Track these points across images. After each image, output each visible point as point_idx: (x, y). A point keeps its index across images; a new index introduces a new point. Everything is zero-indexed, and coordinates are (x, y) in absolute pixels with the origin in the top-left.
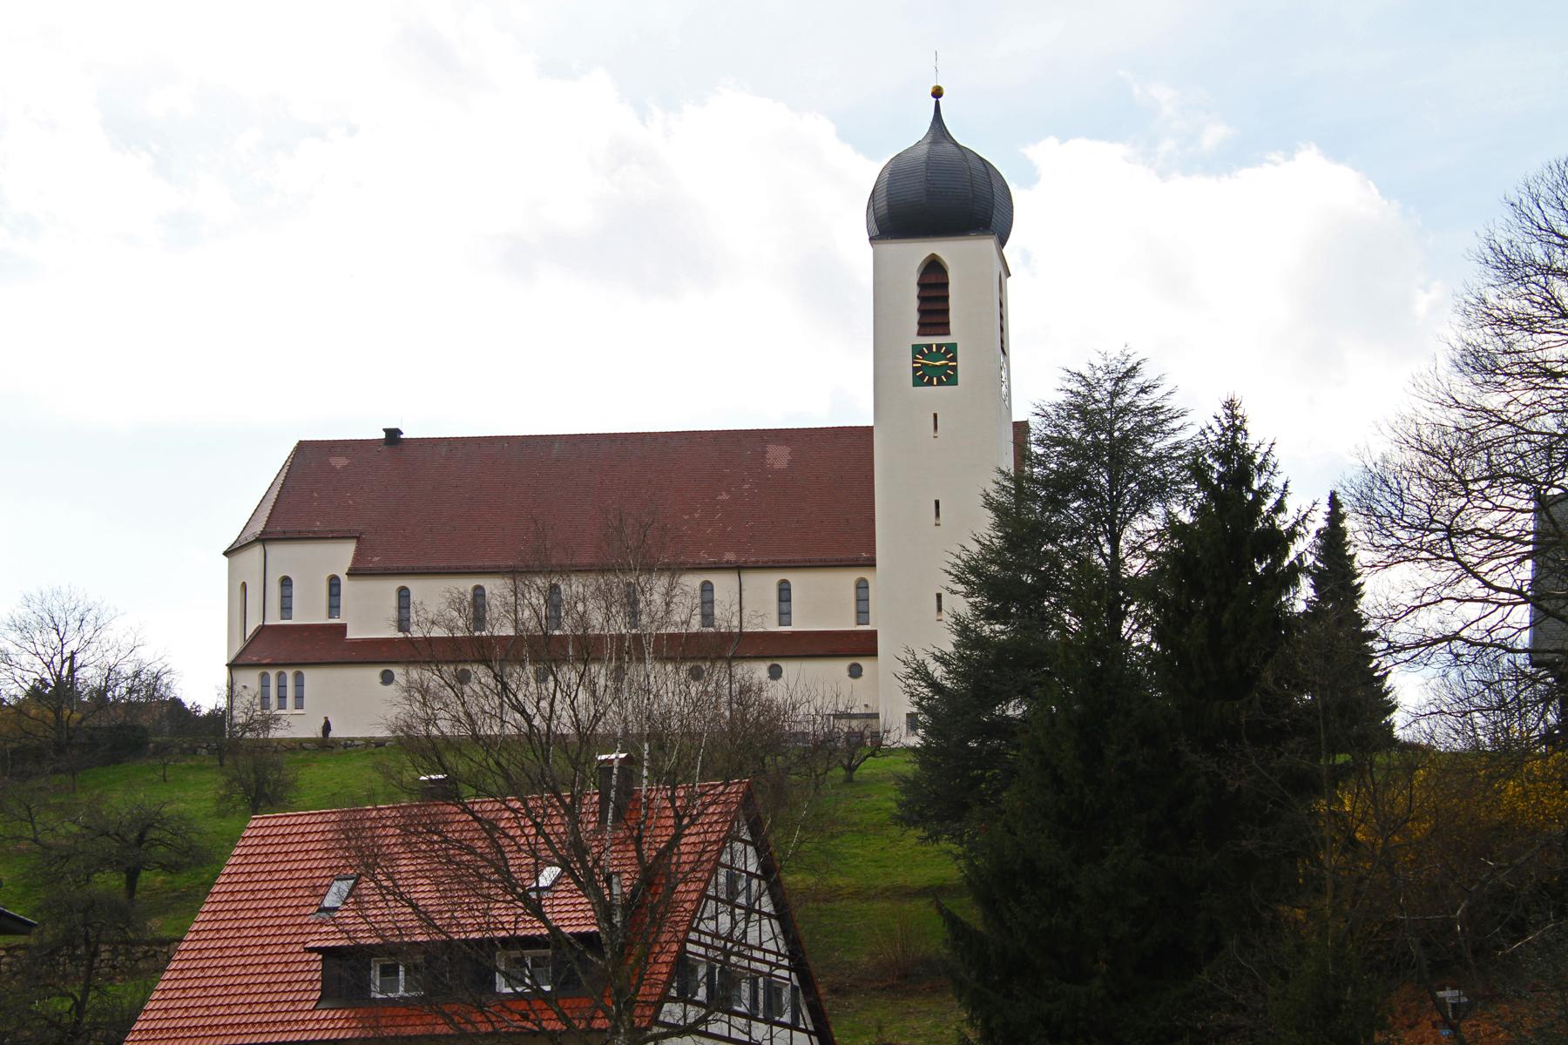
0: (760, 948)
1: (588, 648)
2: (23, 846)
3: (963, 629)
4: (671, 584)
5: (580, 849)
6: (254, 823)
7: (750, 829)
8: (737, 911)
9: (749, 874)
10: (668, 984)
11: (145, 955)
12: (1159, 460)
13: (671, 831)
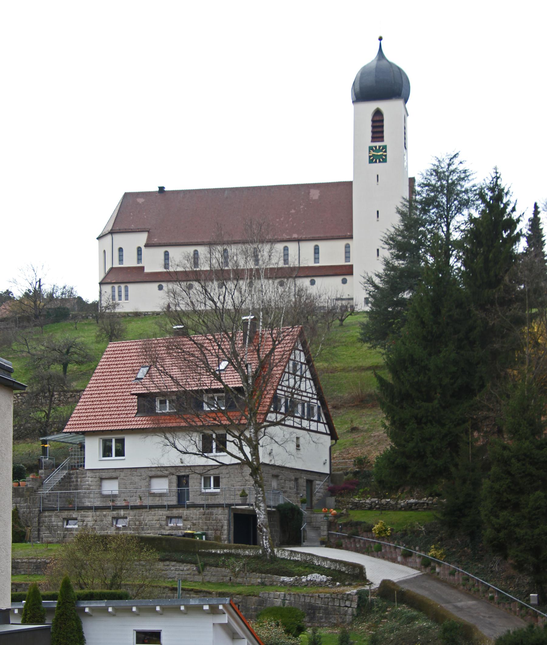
0: (305, 392)
1: (238, 275)
2: (24, 354)
3: (387, 263)
4: (271, 248)
5: (235, 354)
8: (297, 377)
10: (270, 406)
12: (466, 192)
13: (271, 347)
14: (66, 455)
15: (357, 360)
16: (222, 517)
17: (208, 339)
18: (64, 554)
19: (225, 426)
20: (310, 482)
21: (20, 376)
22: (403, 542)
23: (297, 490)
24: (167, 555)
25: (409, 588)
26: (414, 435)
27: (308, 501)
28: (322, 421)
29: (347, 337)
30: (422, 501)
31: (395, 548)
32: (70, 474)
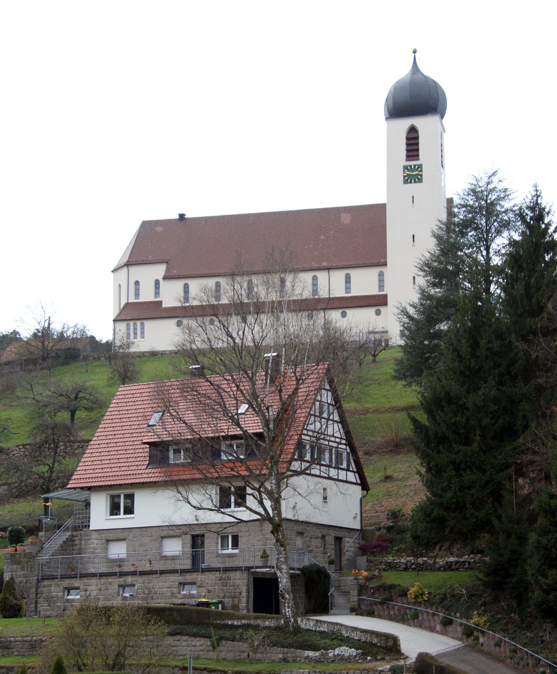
0: (333, 436)
1: (259, 308)
2: (29, 401)
3: (423, 291)
4: (294, 277)
5: (255, 396)
6: (120, 389)
7: (329, 383)
8: (323, 420)
9: (328, 404)
10: (294, 454)
11: (78, 447)
12: (506, 212)
13: (295, 386)
14: (70, 515)
15: (391, 400)
16: (241, 583)
17: (226, 379)
18: (61, 630)
19: (243, 477)
20: (338, 540)
21: (23, 425)
22: (443, 607)
23: (324, 549)
24: (179, 628)
25: (449, 663)
26: (452, 484)
27: (337, 561)
28: (351, 469)
29: (380, 374)
30: (462, 560)
31: (434, 614)
32: (73, 536)
